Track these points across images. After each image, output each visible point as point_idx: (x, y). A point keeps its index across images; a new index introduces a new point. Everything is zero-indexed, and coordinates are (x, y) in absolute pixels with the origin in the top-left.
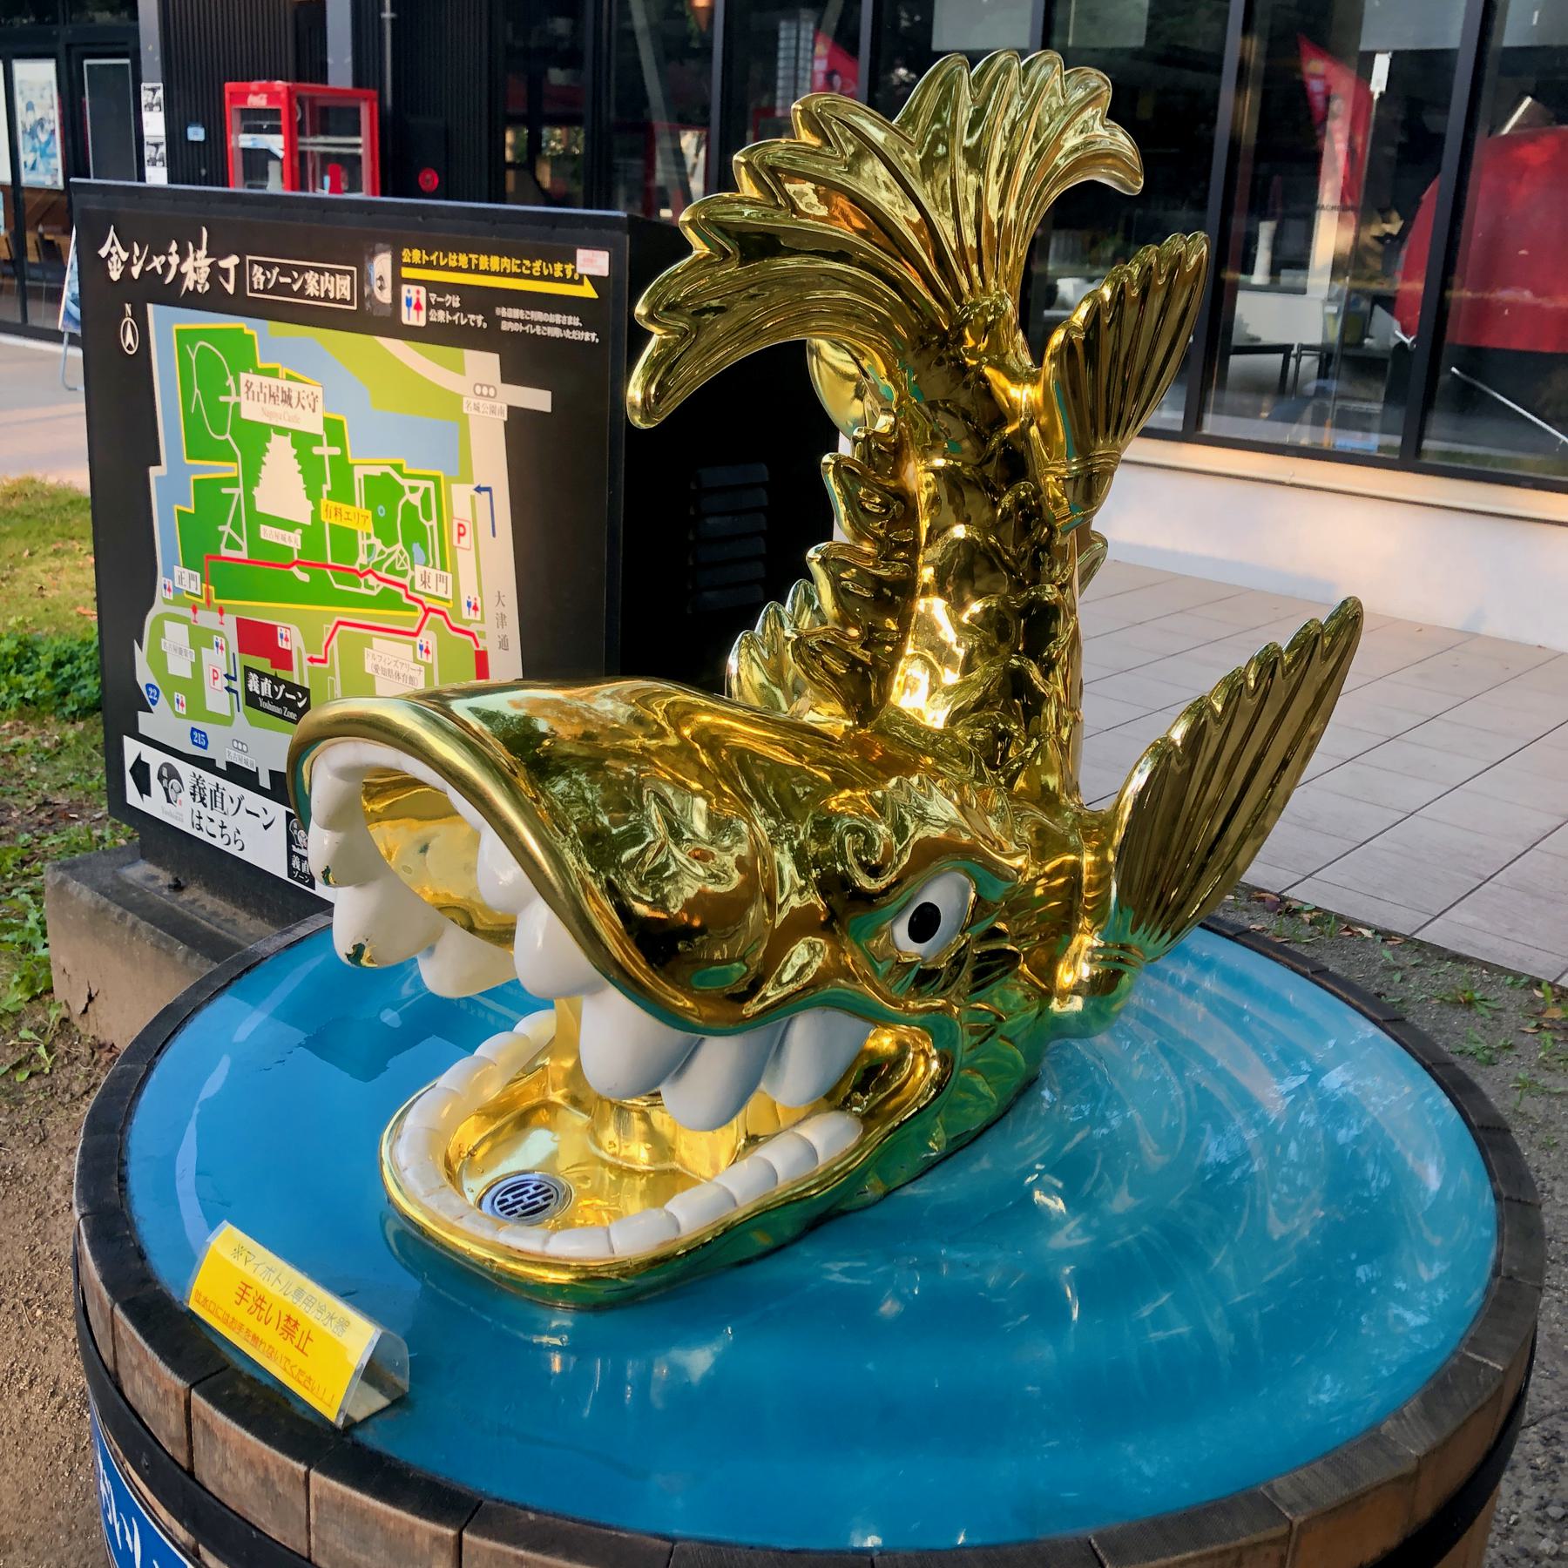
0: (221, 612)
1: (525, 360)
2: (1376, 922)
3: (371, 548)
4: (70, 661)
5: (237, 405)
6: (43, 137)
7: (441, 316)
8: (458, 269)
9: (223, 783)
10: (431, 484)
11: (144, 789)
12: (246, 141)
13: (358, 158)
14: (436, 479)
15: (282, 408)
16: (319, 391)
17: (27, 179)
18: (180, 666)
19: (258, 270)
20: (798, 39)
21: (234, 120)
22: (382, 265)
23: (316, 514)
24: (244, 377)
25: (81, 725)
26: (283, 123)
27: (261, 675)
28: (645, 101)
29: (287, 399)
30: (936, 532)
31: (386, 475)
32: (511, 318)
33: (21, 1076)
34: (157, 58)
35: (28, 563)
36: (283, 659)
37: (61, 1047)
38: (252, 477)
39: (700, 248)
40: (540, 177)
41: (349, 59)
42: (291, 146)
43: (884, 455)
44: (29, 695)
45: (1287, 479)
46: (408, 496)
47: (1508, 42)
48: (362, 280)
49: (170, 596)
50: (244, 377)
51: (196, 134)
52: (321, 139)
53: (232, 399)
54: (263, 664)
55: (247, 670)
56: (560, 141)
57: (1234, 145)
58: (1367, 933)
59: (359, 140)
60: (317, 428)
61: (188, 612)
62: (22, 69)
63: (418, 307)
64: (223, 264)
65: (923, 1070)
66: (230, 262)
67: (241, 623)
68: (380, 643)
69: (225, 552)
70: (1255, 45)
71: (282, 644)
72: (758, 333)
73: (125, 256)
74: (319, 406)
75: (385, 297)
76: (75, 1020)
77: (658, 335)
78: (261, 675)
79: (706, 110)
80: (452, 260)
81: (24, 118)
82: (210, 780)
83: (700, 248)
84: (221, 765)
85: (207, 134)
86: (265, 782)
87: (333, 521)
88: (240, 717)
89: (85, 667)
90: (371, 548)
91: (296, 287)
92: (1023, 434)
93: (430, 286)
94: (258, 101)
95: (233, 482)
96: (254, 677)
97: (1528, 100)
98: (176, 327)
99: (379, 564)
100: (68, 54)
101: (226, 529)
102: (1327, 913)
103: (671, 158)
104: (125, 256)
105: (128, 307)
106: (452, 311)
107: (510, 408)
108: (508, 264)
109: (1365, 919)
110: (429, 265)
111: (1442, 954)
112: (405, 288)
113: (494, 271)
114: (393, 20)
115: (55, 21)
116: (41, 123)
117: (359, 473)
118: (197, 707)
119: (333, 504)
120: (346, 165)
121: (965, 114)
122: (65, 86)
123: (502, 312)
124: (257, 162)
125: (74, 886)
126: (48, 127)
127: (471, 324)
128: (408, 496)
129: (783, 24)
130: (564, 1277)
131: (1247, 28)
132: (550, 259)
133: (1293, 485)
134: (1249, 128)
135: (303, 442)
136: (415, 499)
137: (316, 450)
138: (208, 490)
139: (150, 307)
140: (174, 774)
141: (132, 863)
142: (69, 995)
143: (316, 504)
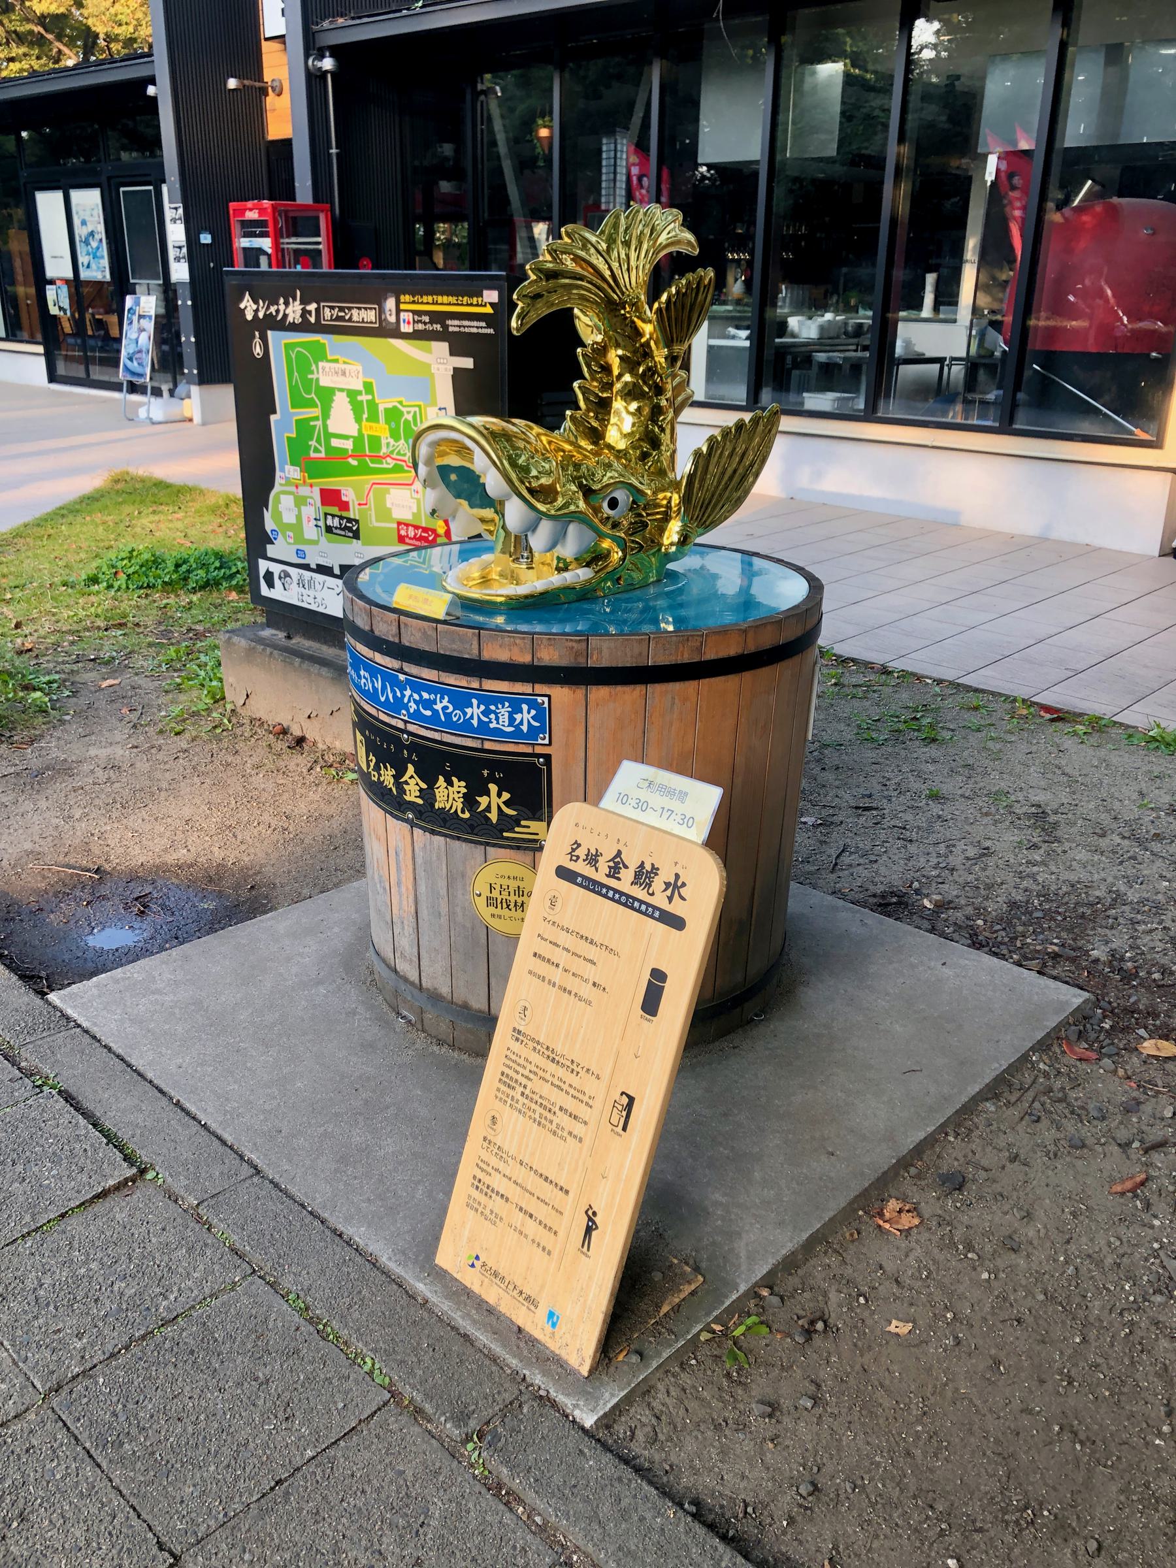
0: (311, 486)
1: (459, 344)
2: (935, 675)
3: (388, 444)
4: (185, 562)
5: (317, 379)
6: (94, 244)
7: (420, 327)
8: (428, 303)
9: (315, 575)
10: (417, 409)
11: (271, 585)
12: (245, 242)
13: (320, 251)
14: (419, 406)
15: (341, 379)
16: (360, 368)
17: (84, 275)
18: (289, 518)
19: (327, 310)
20: (616, 151)
21: (236, 229)
22: (390, 303)
23: (360, 430)
24: (321, 364)
25: (199, 595)
26: (270, 229)
27: (333, 516)
28: (507, 201)
29: (344, 374)
30: (620, 376)
31: (394, 407)
32: (453, 325)
33: (218, 731)
34: (178, 186)
35: (139, 518)
36: (345, 506)
37: (234, 720)
38: (326, 415)
39: (533, 277)
40: (436, 260)
41: (309, 183)
42: (276, 245)
43: (601, 350)
44: (167, 579)
45: (929, 444)
46: (406, 416)
47: (1068, 144)
48: (381, 311)
49: (283, 482)
50: (321, 364)
51: (206, 239)
52: (293, 240)
53: (314, 376)
54: (334, 510)
55: (326, 514)
56: (443, 233)
57: (894, 221)
58: (929, 681)
59: (319, 239)
60: (360, 387)
61: (293, 489)
62: (76, 195)
63: (409, 323)
64: (308, 308)
65: (617, 555)
66: (312, 307)
67: (322, 491)
68: (394, 491)
69: (312, 455)
70: (905, 149)
71: (344, 498)
72: (553, 304)
73: (255, 307)
74: (361, 375)
75: (393, 319)
76: (239, 710)
77: (520, 305)
78: (333, 516)
79: (550, 207)
80: (425, 299)
81: (80, 231)
82: (307, 574)
83: (533, 277)
84: (313, 566)
85: (213, 238)
86: (337, 571)
87: (370, 433)
88: (323, 540)
89: (194, 566)
90: (388, 444)
91: (347, 317)
92: (648, 342)
93: (414, 312)
94: (252, 215)
95: (316, 419)
96: (329, 517)
97: (1090, 182)
98: (284, 342)
99: (392, 452)
100: (109, 186)
101: (313, 443)
102: (907, 672)
103: (527, 243)
104: (255, 307)
105: (257, 333)
106: (425, 323)
107: (455, 369)
108: (452, 299)
109: (929, 674)
110: (414, 302)
111: (969, 689)
112: (402, 314)
113: (445, 303)
114: (337, 154)
115: (99, 161)
116: (92, 234)
117: (381, 408)
118: (299, 537)
119: (369, 424)
120: (313, 256)
121: (622, 229)
122: (108, 204)
123: (449, 322)
124: (252, 255)
125: (235, 639)
126: (97, 237)
127: (435, 329)
128: (406, 416)
129: (604, 141)
130: (502, 599)
131: (901, 139)
132: (471, 296)
133: (933, 447)
134: (903, 209)
135: (352, 394)
136: (410, 417)
137: (359, 398)
138: (303, 425)
139: (269, 332)
140: (287, 575)
141: (263, 629)
142: (235, 697)
143: (360, 425)
